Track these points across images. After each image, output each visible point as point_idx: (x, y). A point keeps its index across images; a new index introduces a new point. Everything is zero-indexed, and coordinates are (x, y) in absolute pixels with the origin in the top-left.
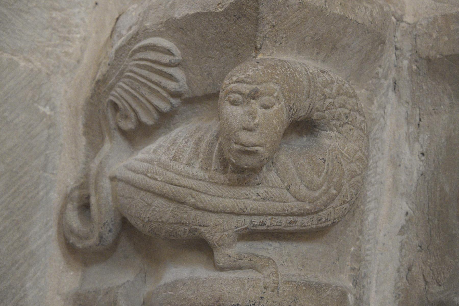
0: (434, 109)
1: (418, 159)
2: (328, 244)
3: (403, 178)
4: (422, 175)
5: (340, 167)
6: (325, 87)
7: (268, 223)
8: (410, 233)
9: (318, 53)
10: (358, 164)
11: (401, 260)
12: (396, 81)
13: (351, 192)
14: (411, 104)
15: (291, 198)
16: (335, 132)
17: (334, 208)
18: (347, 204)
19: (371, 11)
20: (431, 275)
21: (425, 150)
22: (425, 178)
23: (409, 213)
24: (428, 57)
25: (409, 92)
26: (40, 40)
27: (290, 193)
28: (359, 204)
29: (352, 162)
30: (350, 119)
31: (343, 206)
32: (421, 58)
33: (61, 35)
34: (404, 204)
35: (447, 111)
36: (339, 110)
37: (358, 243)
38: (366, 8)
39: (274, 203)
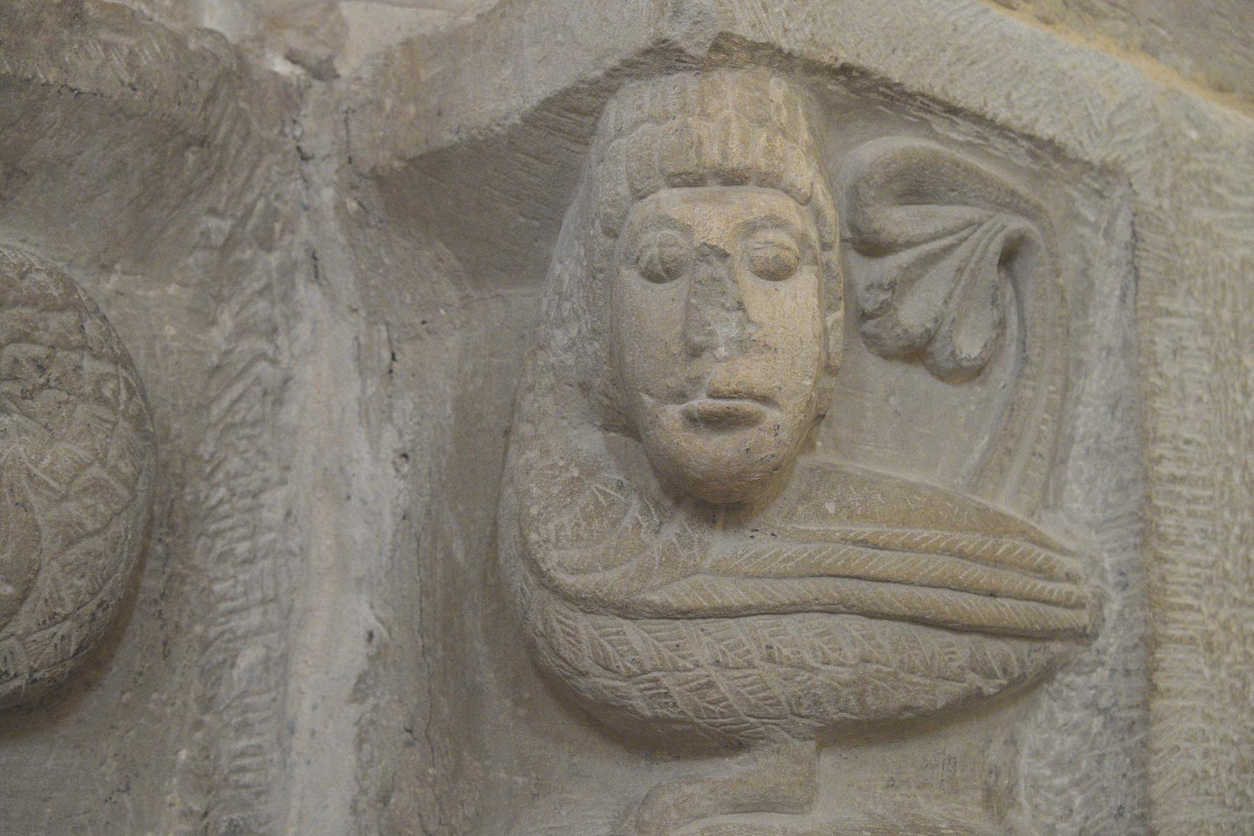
0: (424, 322)
1: (393, 472)
2: (77, 747)
3: (359, 533)
4: (404, 518)
8: (383, 693)
10: (88, 501)
11: (360, 775)
12: (314, 252)
13: (71, 586)
14: (363, 313)
16: (16, 417)
18: (69, 623)
19: (131, 52)
20: (437, 813)
21: (409, 446)
22: (411, 526)
23: (375, 633)
24: (373, 170)
25: (352, 279)
28: (184, 622)
29: (65, 498)
30: (55, 372)
31: (54, 629)
32: (361, 175)
34: (365, 610)
35: (457, 322)
37: (198, 735)
38: (107, 47)
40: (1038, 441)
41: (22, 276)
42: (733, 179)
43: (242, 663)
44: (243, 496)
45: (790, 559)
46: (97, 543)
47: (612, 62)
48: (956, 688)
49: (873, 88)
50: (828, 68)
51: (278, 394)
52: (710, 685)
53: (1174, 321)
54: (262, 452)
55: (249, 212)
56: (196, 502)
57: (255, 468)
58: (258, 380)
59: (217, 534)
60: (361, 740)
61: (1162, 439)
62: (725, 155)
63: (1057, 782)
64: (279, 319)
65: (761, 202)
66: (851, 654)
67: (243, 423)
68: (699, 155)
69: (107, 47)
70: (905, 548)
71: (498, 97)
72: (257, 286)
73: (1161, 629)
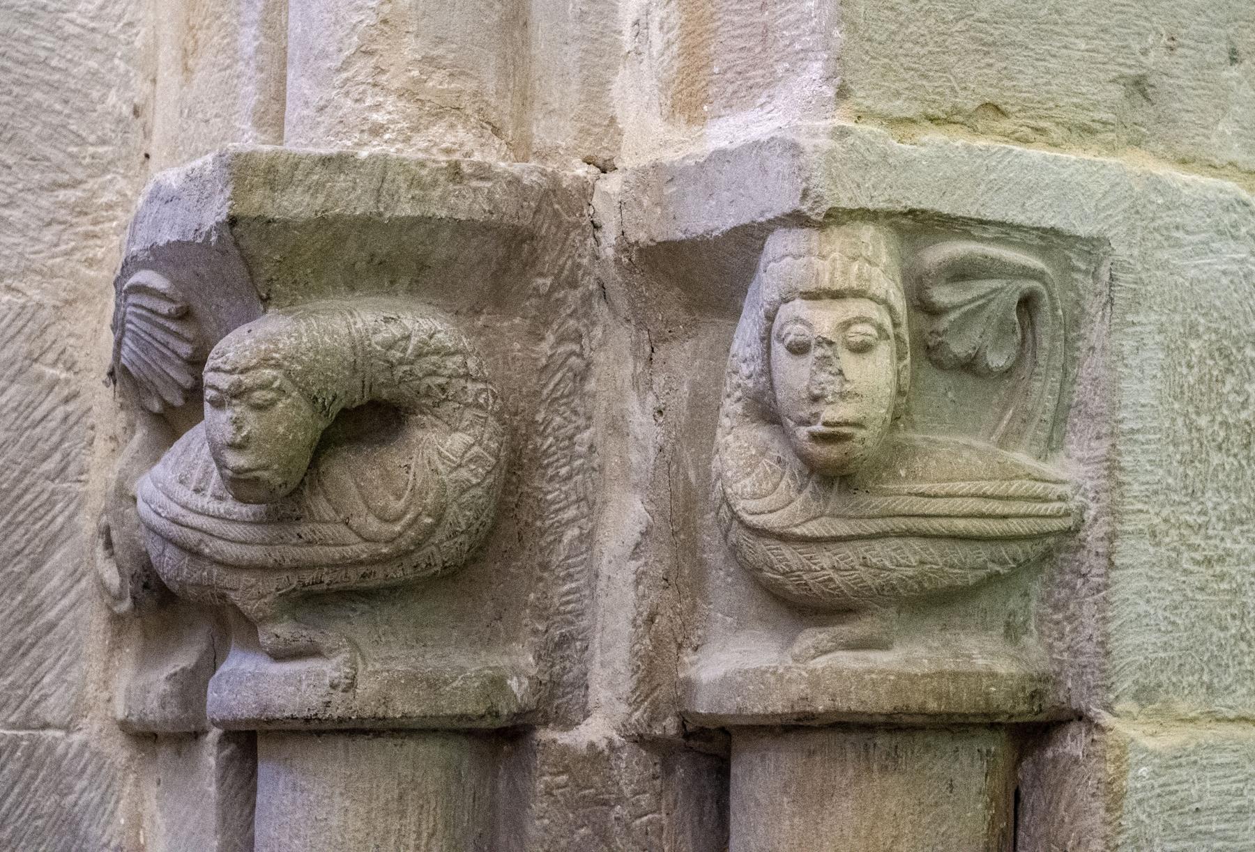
3: (635, 457)
5: (436, 477)
6: (390, 347)
7: (327, 579)
9: (392, 282)
14: (633, 322)
15: (353, 538)
17: (437, 546)
26: (37, 248)
27: (350, 528)
29: (460, 466)
33: (79, 229)
36: (428, 381)
39: (327, 549)
40: (1044, 413)
41: (431, 337)
42: (837, 295)
43: (566, 540)
44: (563, 440)
45: (877, 507)
46: (479, 491)
47: (770, 216)
48: (982, 573)
49: (931, 218)
50: (901, 213)
51: (582, 376)
52: (831, 580)
53: (1139, 328)
54: (575, 413)
55: (562, 268)
56: (535, 450)
57: (570, 422)
58: (570, 369)
59: (548, 465)
60: (637, 583)
61: (1126, 406)
62: (831, 280)
63: (1055, 617)
64: (583, 329)
65: (854, 308)
66: (913, 560)
67: (562, 396)
68: (817, 281)
69: (475, 190)
70: (948, 495)
71: (708, 217)
72: (569, 311)
73: (1119, 527)
